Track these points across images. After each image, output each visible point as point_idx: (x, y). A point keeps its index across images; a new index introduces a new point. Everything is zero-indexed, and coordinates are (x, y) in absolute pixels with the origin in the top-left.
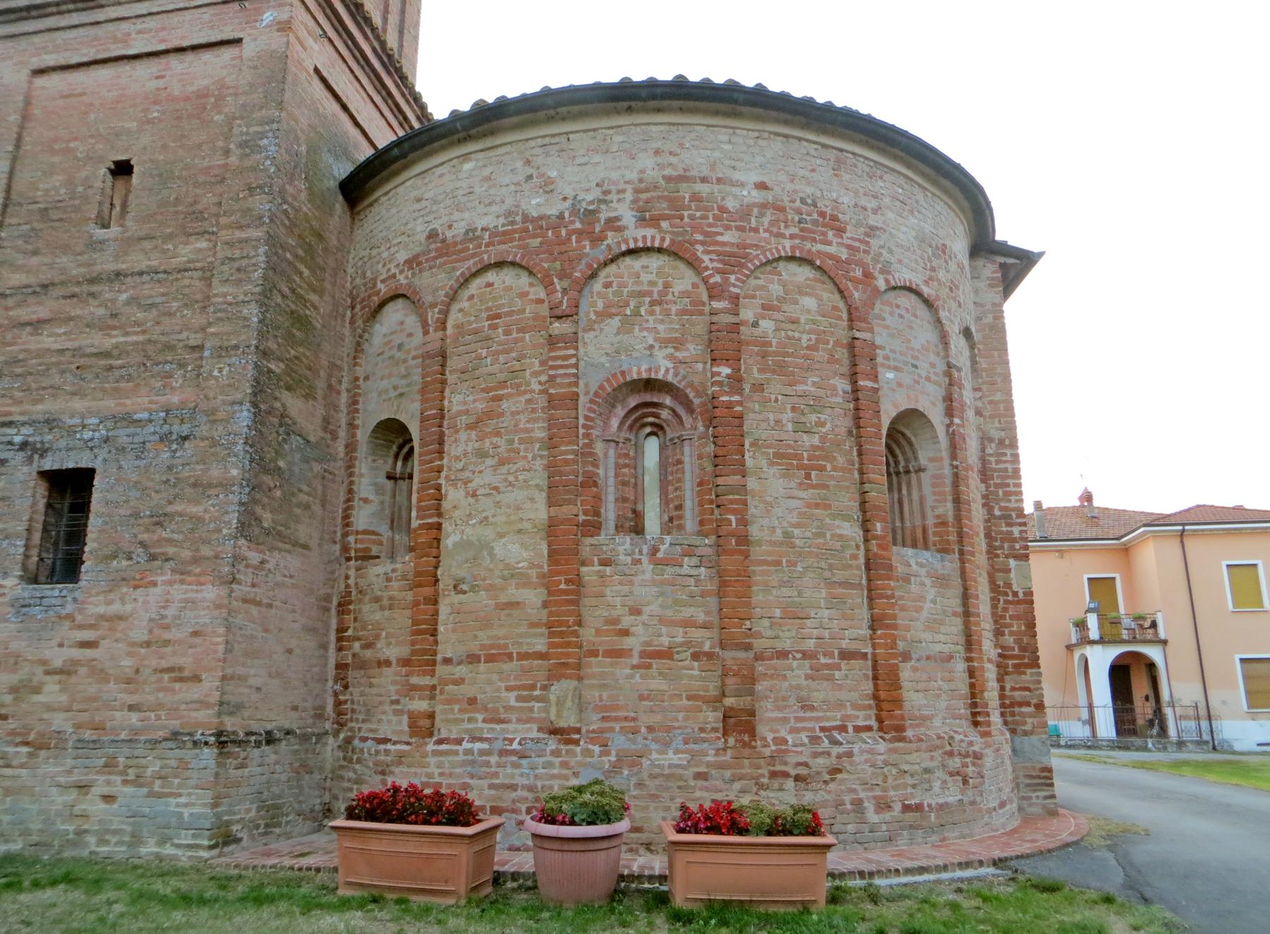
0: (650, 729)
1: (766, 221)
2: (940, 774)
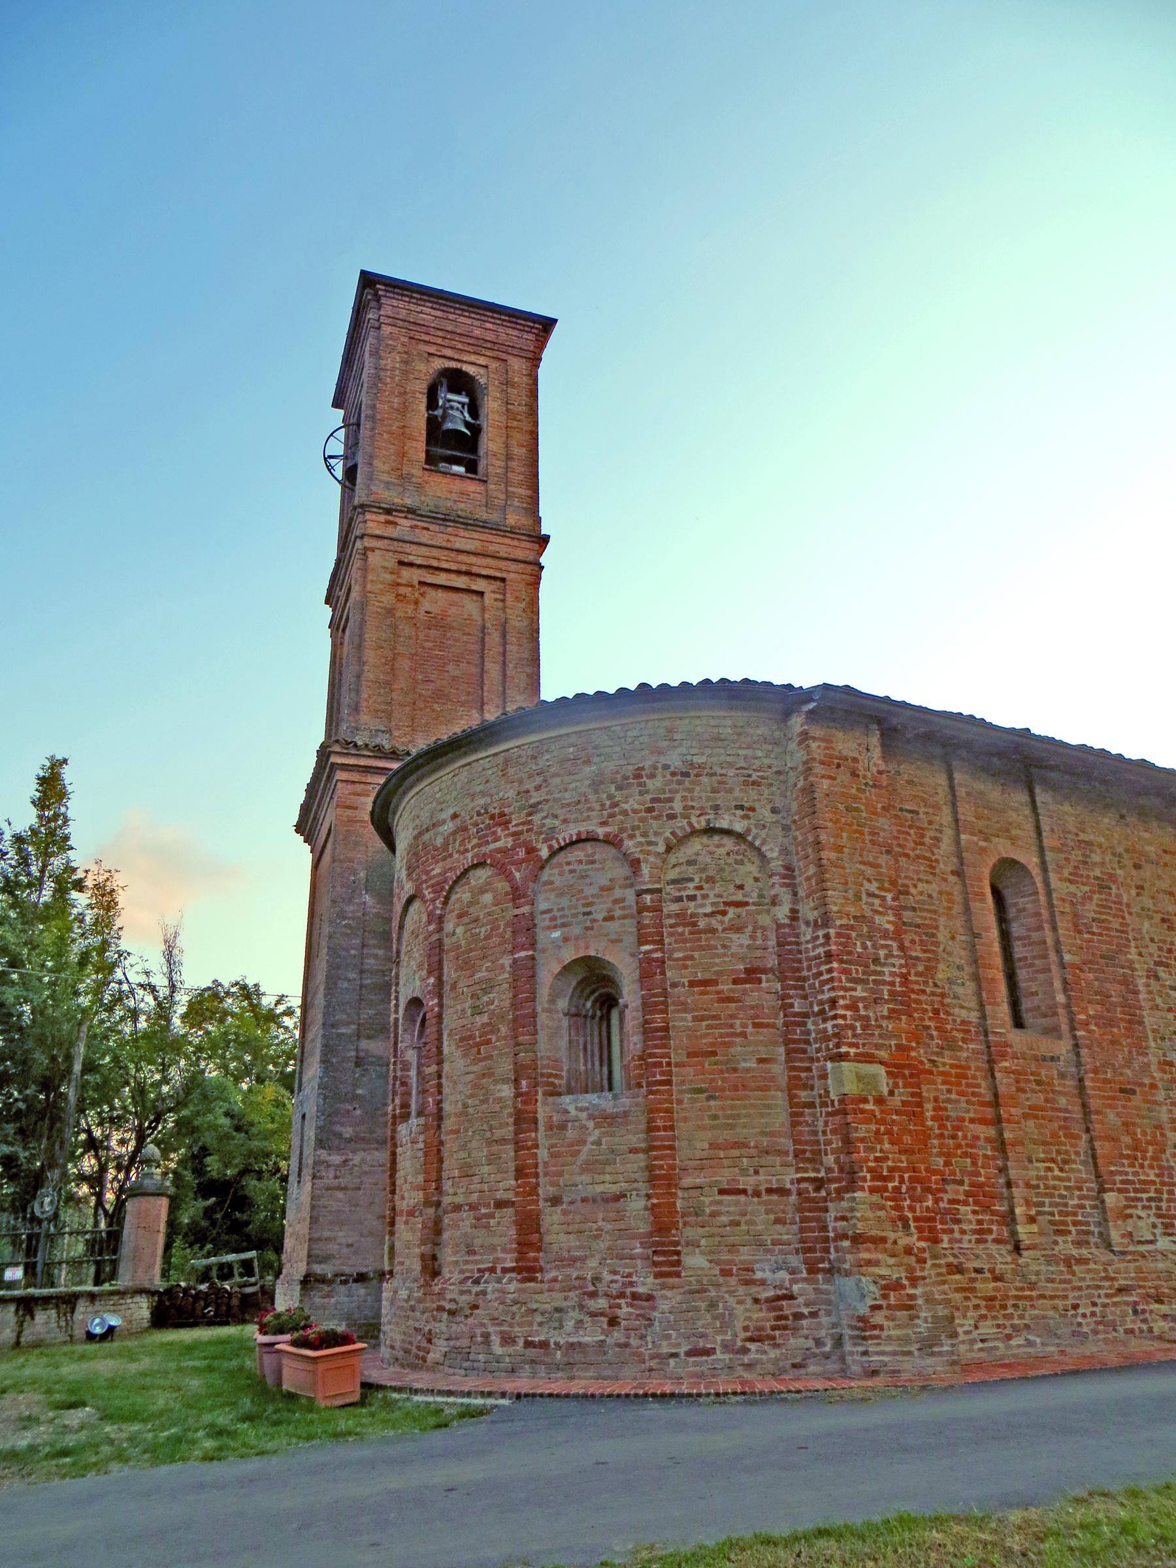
2: (575, 1314)
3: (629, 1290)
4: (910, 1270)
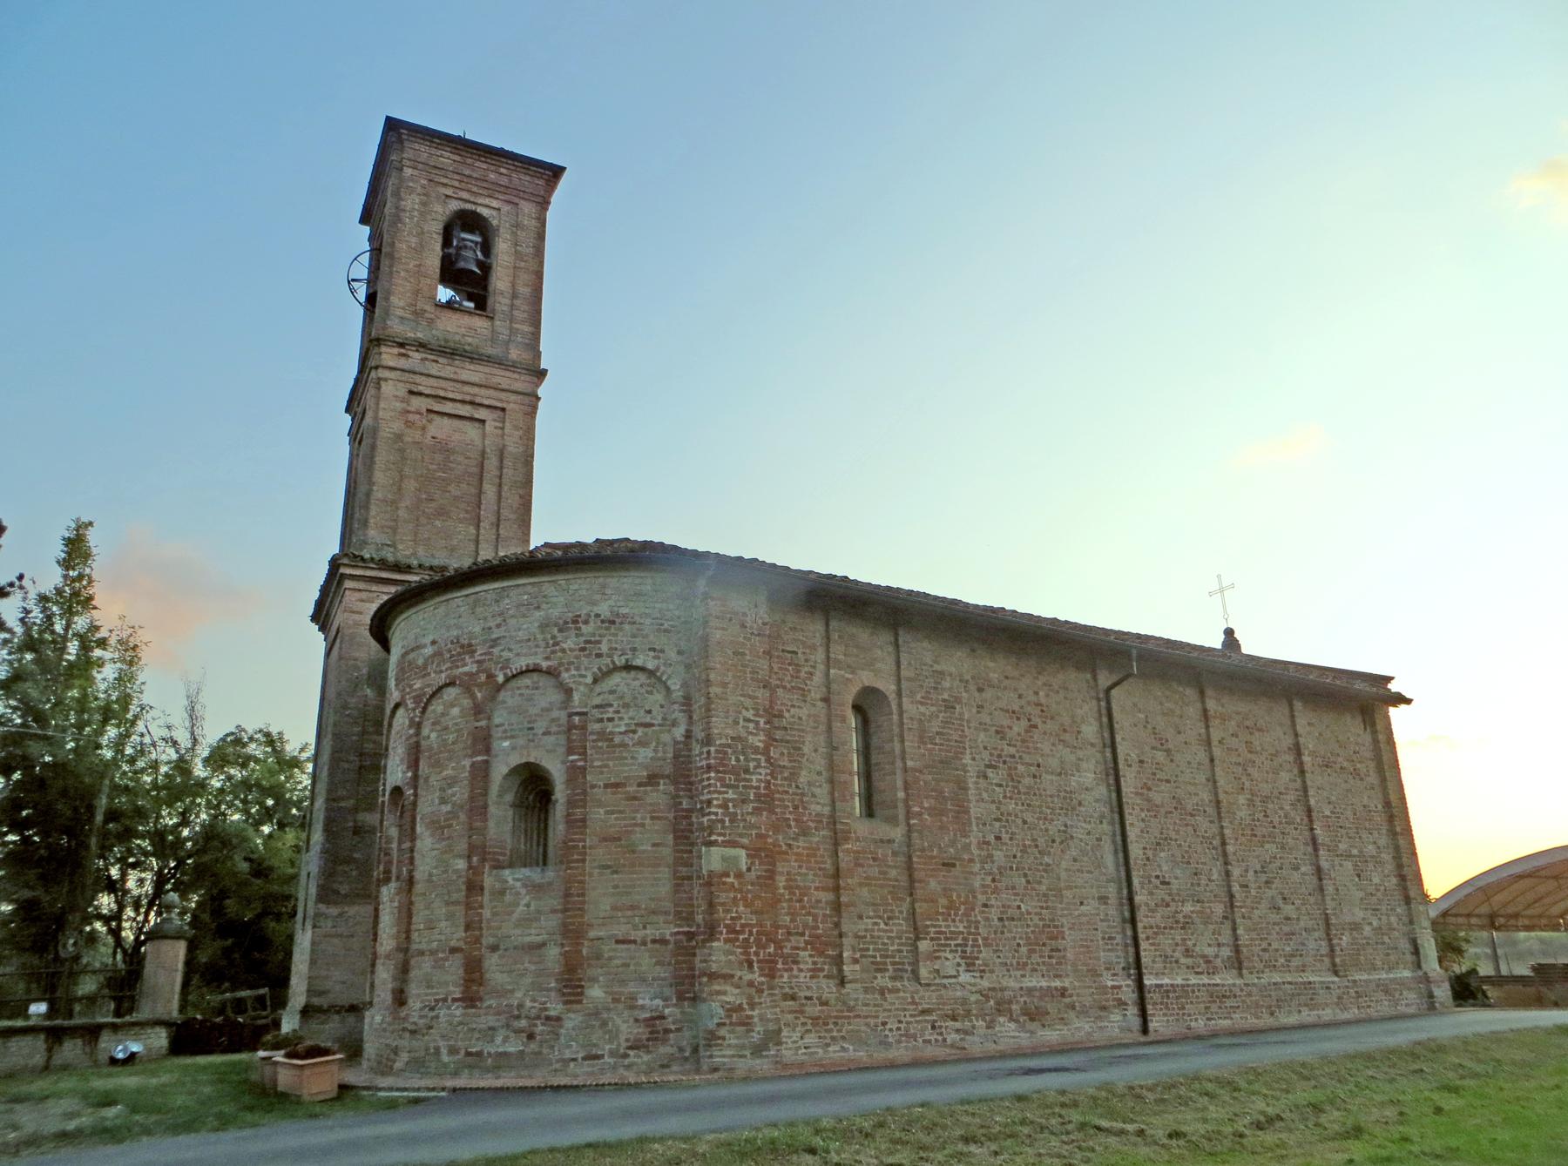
4: (750, 998)
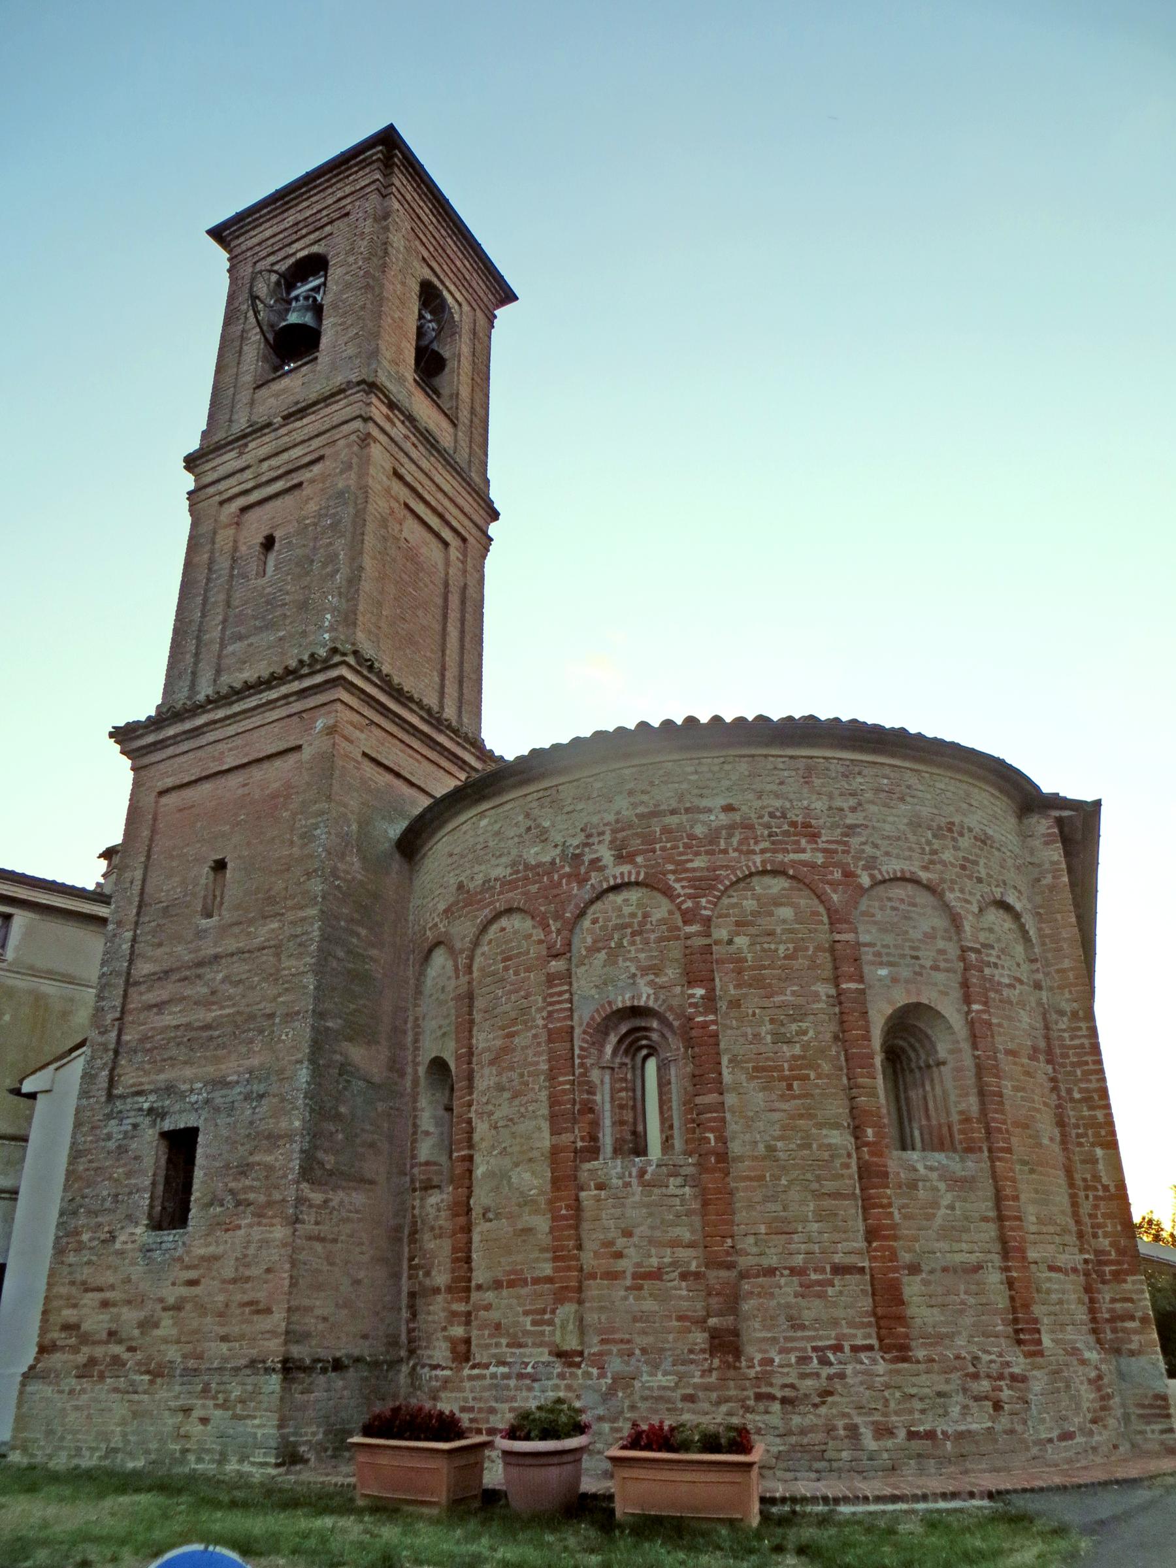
0: (644, 1351)
1: (735, 841)
2: (960, 1398)
3: (1007, 1371)
